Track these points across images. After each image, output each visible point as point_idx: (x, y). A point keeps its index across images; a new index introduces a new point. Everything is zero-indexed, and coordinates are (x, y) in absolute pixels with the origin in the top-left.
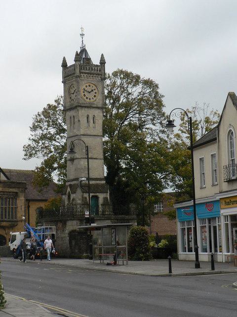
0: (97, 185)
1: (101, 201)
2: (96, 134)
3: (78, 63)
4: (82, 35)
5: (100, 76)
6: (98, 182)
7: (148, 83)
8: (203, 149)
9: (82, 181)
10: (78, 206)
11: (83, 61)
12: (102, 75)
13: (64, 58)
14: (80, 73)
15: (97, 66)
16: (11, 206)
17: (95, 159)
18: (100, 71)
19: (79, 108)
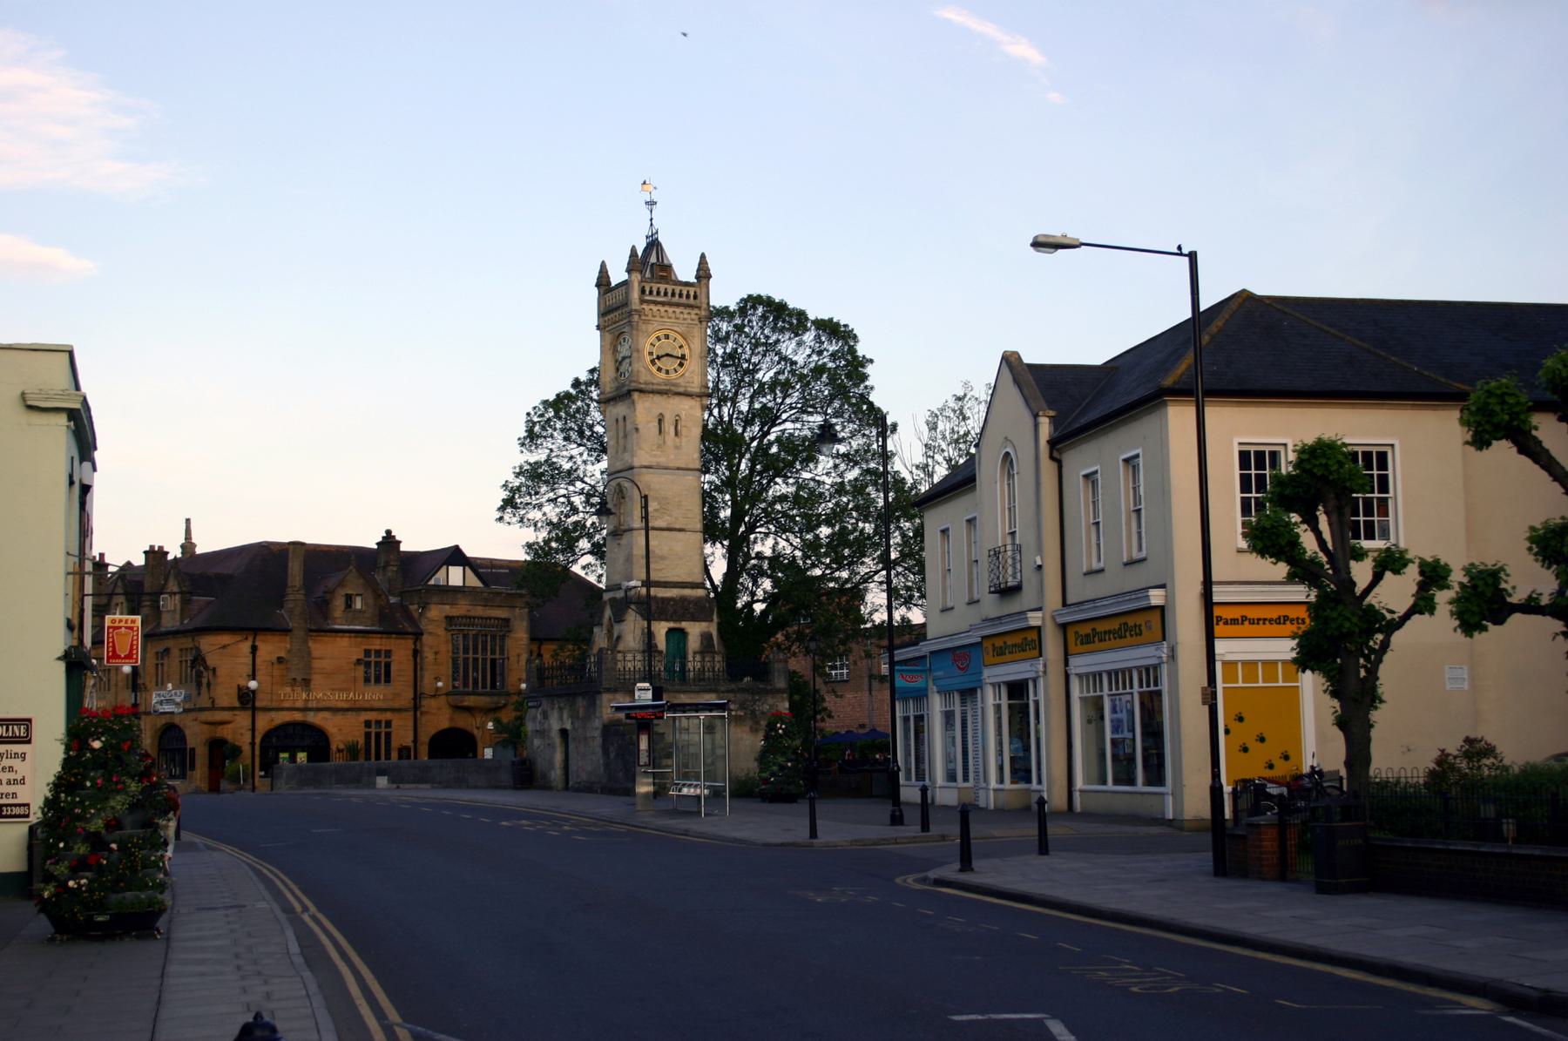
0: (683, 599)
1: (693, 643)
2: (683, 466)
3: (636, 277)
4: (651, 204)
5: (696, 311)
6: (687, 592)
7: (830, 329)
8: (944, 505)
9: (630, 589)
10: (629, 657)
11: (652, 271)
12: (699, 308)
13: (603, 265)
14: (642, 301)
15: (687, 284)
16: (489, 656)
17: (680, 530)
18: (695, 297)
19: (636, 395)
